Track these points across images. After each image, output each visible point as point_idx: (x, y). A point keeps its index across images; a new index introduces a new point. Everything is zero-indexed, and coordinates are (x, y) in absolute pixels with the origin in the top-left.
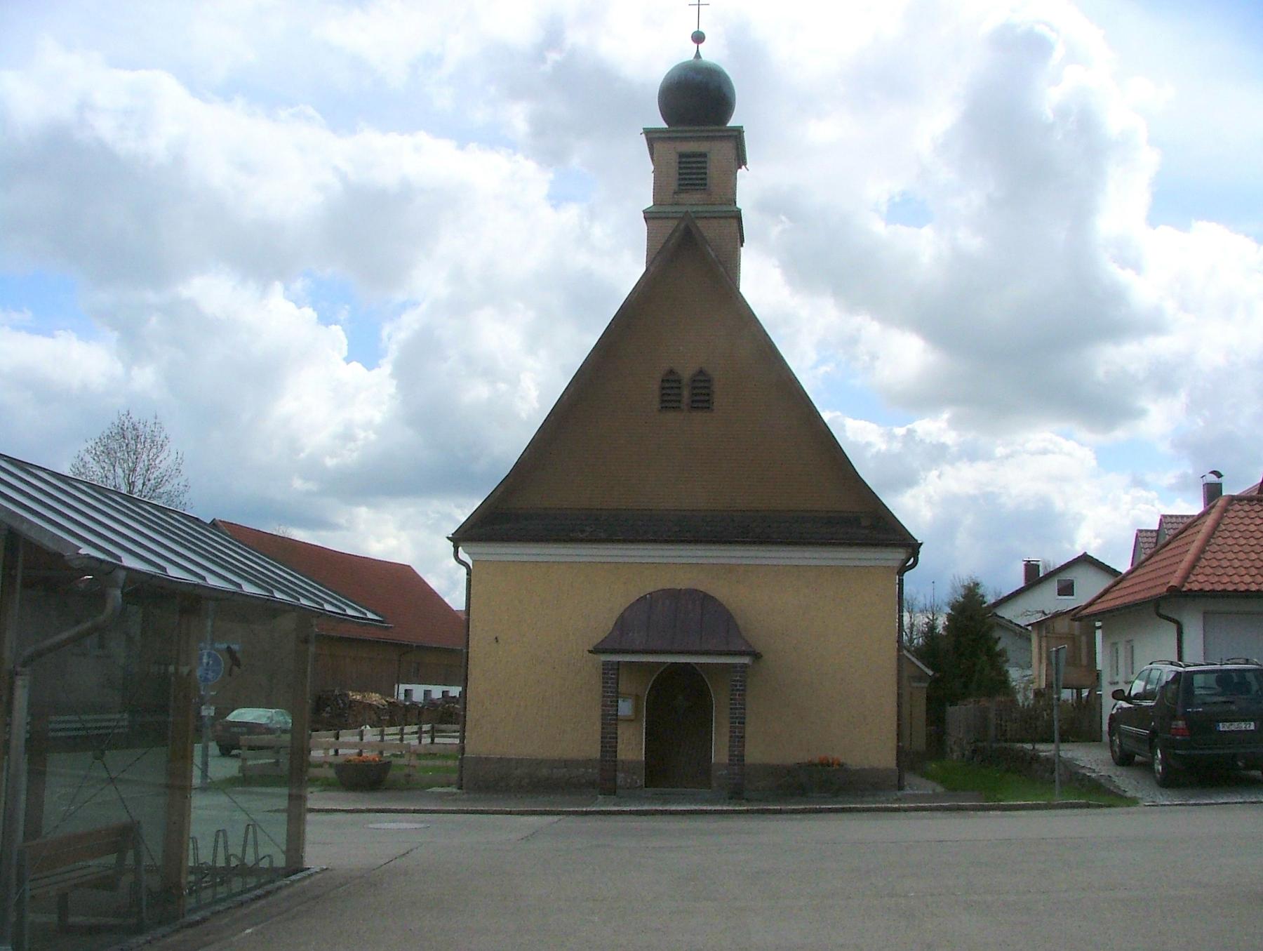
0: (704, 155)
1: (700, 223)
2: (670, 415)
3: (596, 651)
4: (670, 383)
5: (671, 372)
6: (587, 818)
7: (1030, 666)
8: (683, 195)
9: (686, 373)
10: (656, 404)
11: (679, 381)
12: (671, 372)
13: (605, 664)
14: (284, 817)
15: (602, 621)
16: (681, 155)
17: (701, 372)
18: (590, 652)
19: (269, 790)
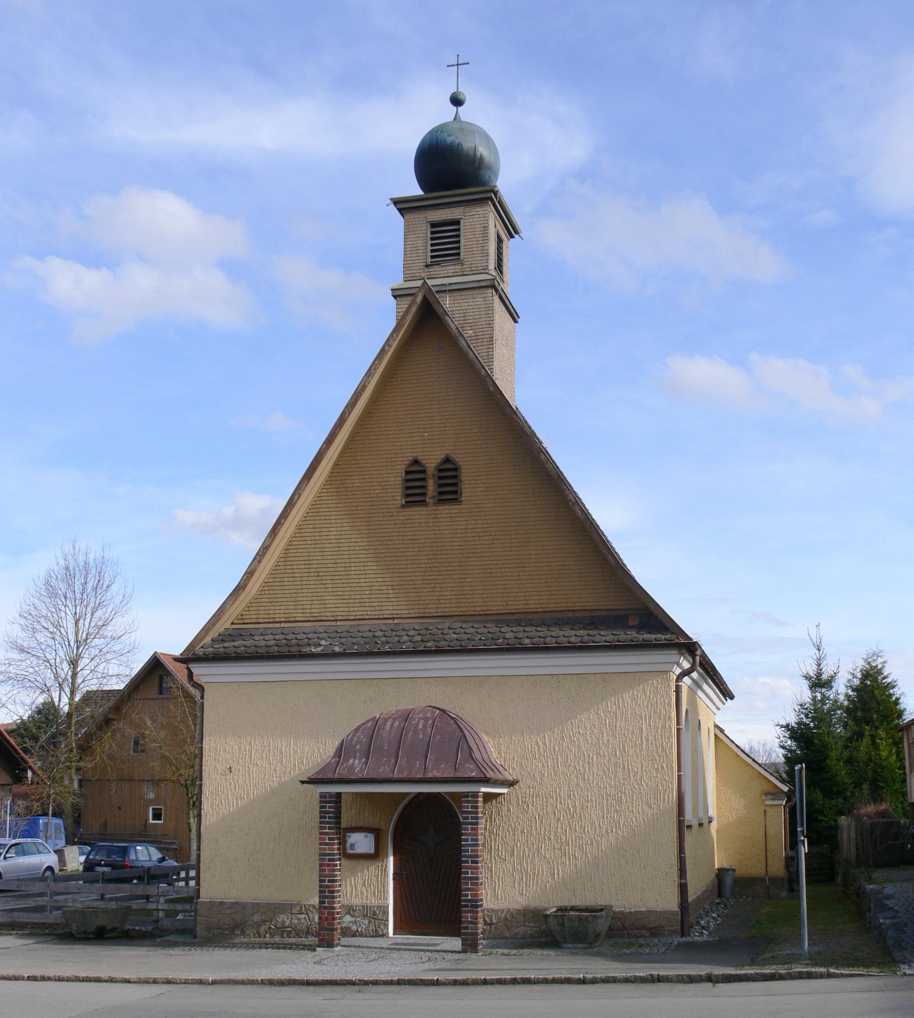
0: (457, 222)
1: (447, 302)
2: (417, 512)
3: (311, 781)
4: (415, 473)
5: (416, 462)
6: (320, 989)
7: (154, 819)
8: (436, 268)
9: (432, 463)
10: (400, 500)
11: (424, 472)
12: (416, 462)
13: (323, 796)
14: (763, 873)
15: (317, 752)
16: (433, 225)
17: (448, 460)
18: (303, 782)
19: (667, 965)
